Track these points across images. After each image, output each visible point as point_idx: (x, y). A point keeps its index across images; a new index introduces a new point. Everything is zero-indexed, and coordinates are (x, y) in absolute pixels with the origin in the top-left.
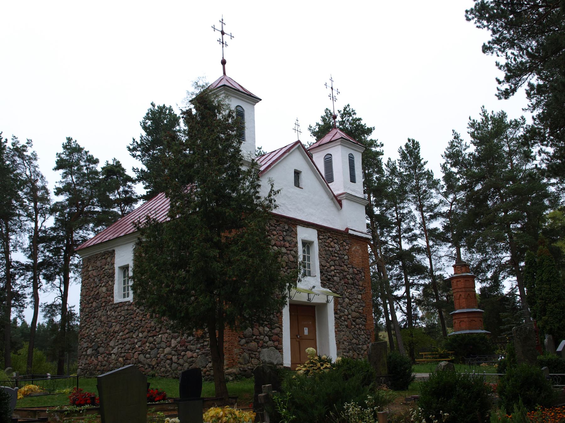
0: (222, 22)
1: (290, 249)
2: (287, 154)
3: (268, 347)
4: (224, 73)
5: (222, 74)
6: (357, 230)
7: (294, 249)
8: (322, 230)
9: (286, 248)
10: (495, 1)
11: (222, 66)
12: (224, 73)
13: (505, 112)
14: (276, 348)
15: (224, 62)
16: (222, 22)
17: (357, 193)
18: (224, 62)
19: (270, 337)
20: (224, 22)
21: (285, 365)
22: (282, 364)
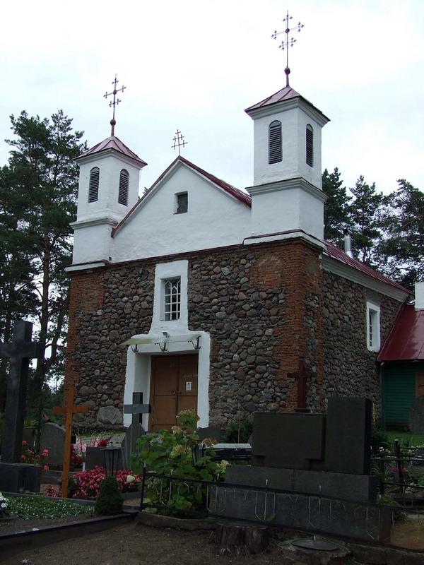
0: (124, 88)
1: (145, 294)
2: (196, 172)
3: (105, 406)
4: (113, 134)
5: (110, 135)
6: (257, 235)
7: (150, 293)
8: (193, 258)
9: (139, 295)
10: (396, 365)
11: (286, 75)
12: (113, 134)
13: (42, 112)
14: (116, 406)
15: (287, 71)
16: (124, 88)
17: (281, 175)
18: (287, 71)
19: (109, 395)
20: (124, 90)
21: (125, 426)
22: (123, 424)
